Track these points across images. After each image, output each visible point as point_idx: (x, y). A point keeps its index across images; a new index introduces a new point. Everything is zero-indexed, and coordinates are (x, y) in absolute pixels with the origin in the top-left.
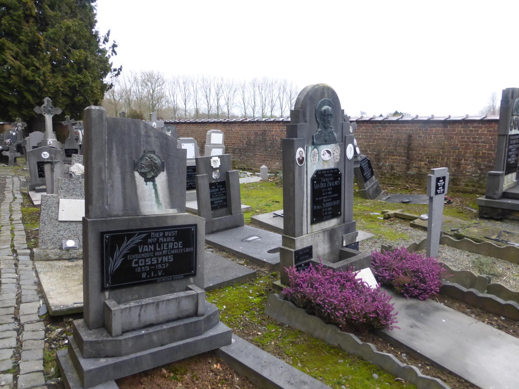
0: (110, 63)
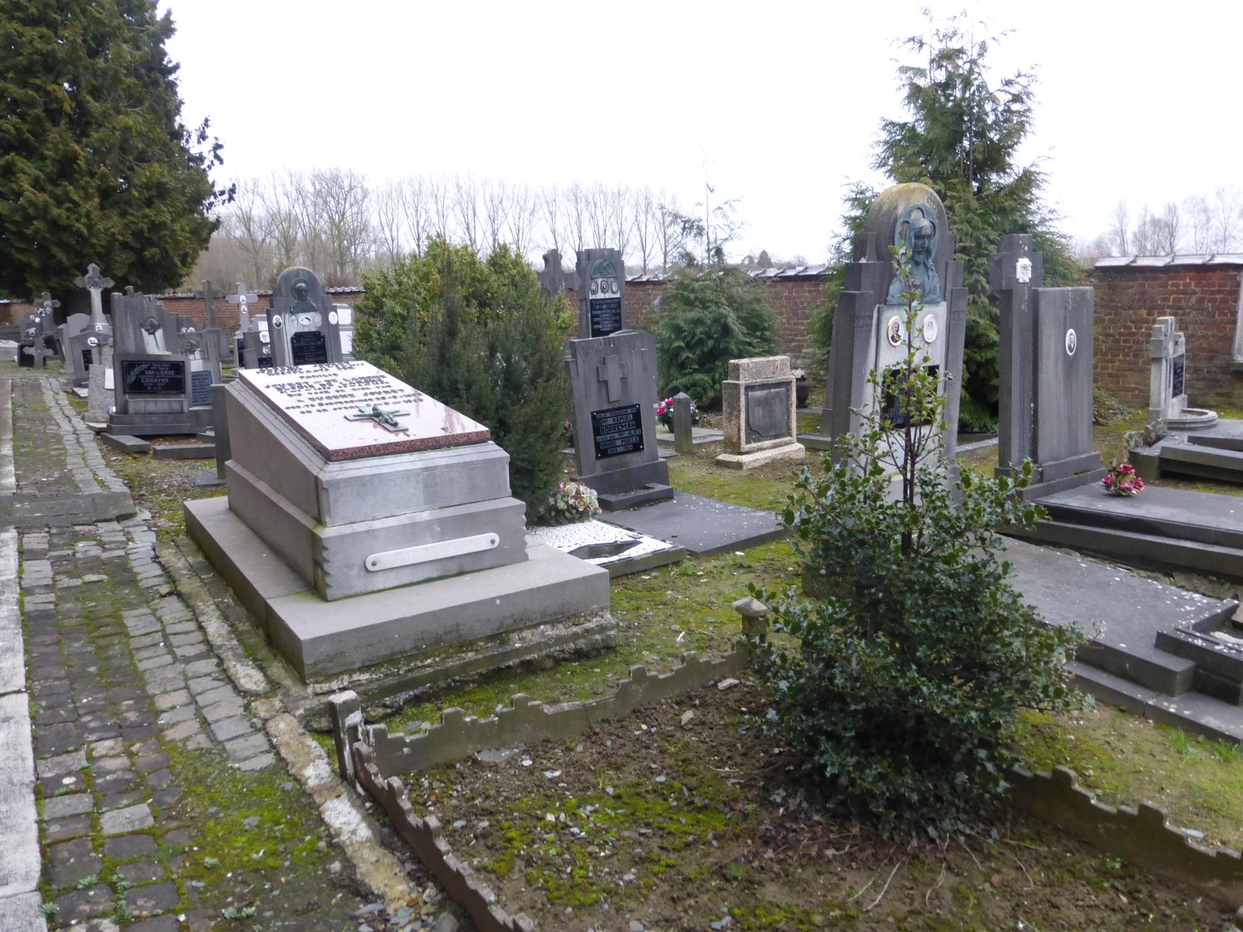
0: (210, 180)
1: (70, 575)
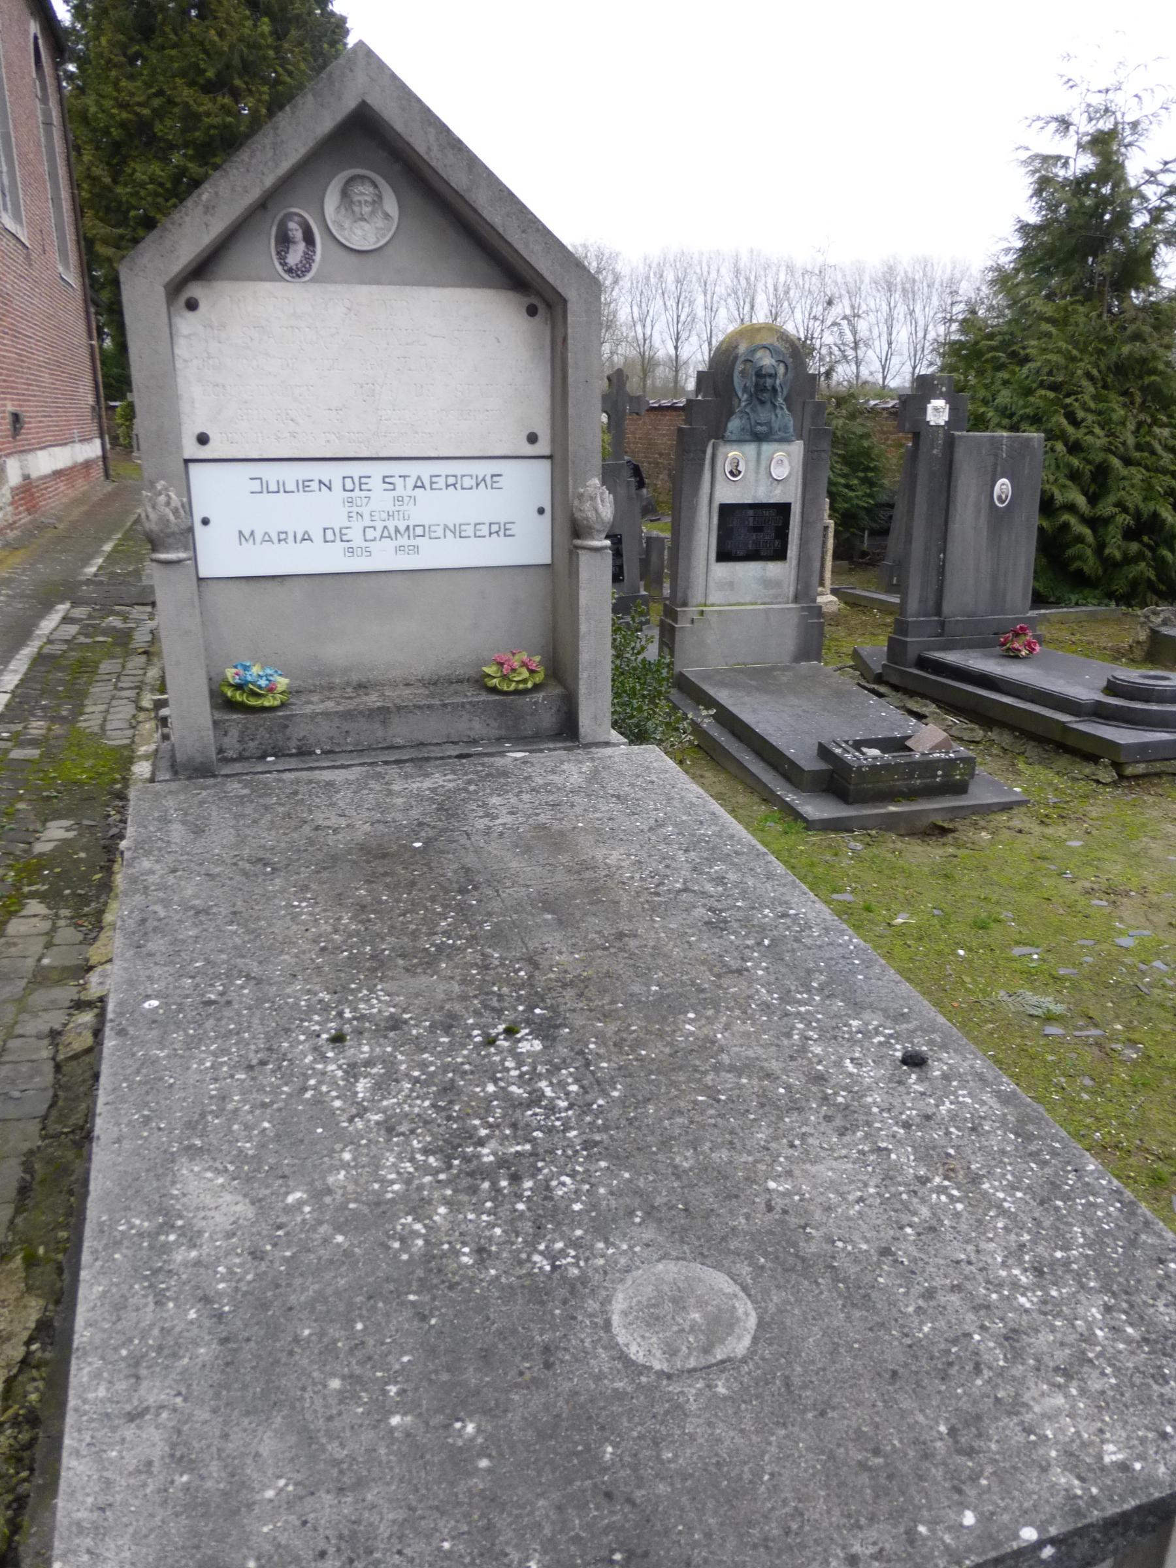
1: (87, 636)
